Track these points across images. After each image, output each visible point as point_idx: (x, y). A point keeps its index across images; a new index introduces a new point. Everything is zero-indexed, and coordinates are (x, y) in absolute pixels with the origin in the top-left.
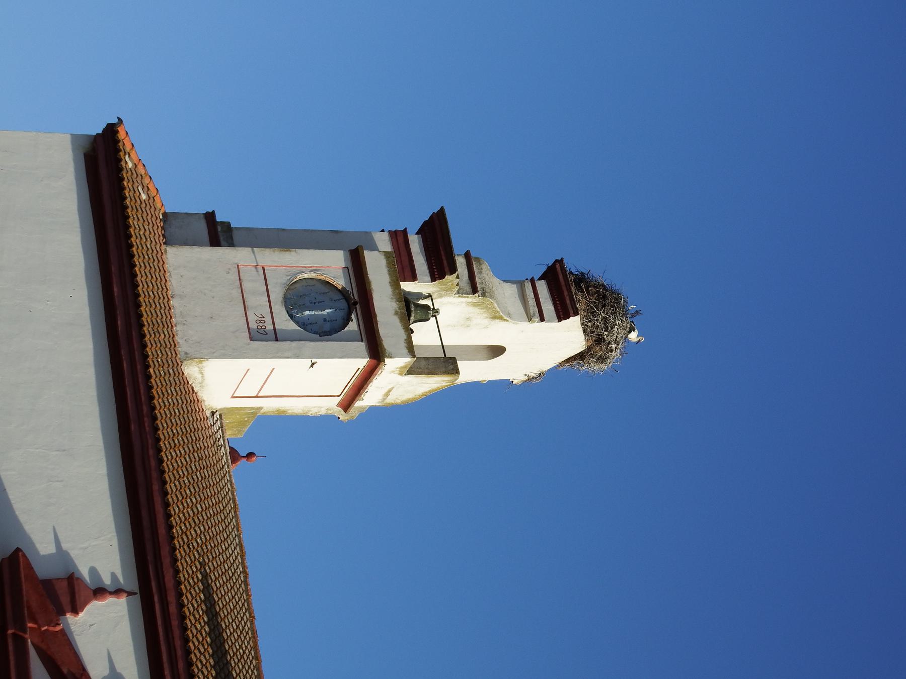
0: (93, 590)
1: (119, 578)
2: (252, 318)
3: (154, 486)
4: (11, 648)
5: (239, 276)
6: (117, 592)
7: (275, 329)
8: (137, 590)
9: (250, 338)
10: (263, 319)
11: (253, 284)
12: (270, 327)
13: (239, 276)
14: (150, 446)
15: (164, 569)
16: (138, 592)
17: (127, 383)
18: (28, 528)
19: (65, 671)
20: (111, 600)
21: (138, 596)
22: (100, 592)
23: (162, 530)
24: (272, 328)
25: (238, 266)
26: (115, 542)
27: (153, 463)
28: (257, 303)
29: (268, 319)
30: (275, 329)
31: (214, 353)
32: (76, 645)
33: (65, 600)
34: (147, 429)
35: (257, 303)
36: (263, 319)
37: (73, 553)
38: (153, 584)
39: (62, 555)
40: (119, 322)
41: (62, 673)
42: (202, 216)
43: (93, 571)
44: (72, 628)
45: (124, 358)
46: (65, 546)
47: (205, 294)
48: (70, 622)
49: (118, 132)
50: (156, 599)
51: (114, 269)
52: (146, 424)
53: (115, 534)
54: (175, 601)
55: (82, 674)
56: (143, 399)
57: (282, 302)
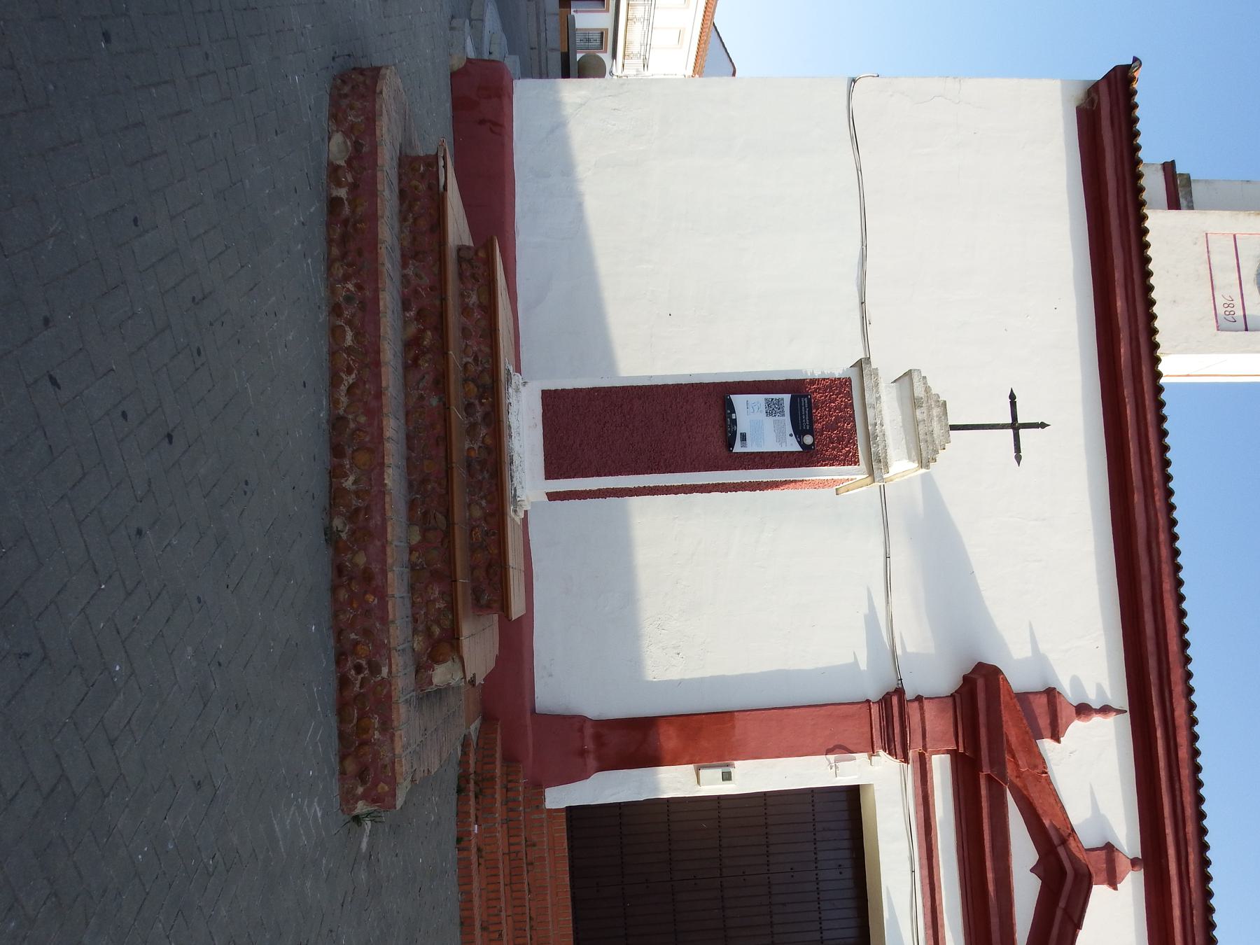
0: (1075, 707)
1: (1106, 691)
2: (1220, 301)
3: (1164, 585)
4: (984, 792)
5: (1208, 247)
6: (1105, 710)
7: (1245, 316)
8: (1127, 708)
9: (1218, 327)
10: (1232, 302)
11: (1222, 258)
12: (1239, 313)
13: (1208, 247)
14: (1161, 530)
15: (1174, 700)
16: (1128, 711)
17: (1130, 435)
18: (999, 623)
19: (1047, 822)
20: (1097, 719)
21: (1127, 715)
22: (1083, 710)
23: (1173, 646)
24: (1241, 313)
25: (1207, 234)
26: (1102, 643)
27: (1165, 552)
28: (1226, 279)
29: (1238, 302)
30: (1245, 316)
31: (1176, 346)
32: (1054, 778)
33: (1044, 722)
34: (1158, 504)
35: (1226, 279)
36: (1232, 302)
37: (1052, 657)
38: (1157, 714)
39: (1039, 658)
40: (1122, 351)
41: (1042, 825)
42: (1160, 167)
43: (1076, 682)
44: (1049, 755)
45: (1127, 400)
46: (1043, 647)
47: (1168, 272)
48: (1047, 748)
49: (1133, 79)
50: (1159, 733)
51: (1118, 275)
52: (1157, 498)
53: (1102, 632)
54: (1186, 743)
55: (1070, 834)
56: (1154, 462)
57: (1254, 281)
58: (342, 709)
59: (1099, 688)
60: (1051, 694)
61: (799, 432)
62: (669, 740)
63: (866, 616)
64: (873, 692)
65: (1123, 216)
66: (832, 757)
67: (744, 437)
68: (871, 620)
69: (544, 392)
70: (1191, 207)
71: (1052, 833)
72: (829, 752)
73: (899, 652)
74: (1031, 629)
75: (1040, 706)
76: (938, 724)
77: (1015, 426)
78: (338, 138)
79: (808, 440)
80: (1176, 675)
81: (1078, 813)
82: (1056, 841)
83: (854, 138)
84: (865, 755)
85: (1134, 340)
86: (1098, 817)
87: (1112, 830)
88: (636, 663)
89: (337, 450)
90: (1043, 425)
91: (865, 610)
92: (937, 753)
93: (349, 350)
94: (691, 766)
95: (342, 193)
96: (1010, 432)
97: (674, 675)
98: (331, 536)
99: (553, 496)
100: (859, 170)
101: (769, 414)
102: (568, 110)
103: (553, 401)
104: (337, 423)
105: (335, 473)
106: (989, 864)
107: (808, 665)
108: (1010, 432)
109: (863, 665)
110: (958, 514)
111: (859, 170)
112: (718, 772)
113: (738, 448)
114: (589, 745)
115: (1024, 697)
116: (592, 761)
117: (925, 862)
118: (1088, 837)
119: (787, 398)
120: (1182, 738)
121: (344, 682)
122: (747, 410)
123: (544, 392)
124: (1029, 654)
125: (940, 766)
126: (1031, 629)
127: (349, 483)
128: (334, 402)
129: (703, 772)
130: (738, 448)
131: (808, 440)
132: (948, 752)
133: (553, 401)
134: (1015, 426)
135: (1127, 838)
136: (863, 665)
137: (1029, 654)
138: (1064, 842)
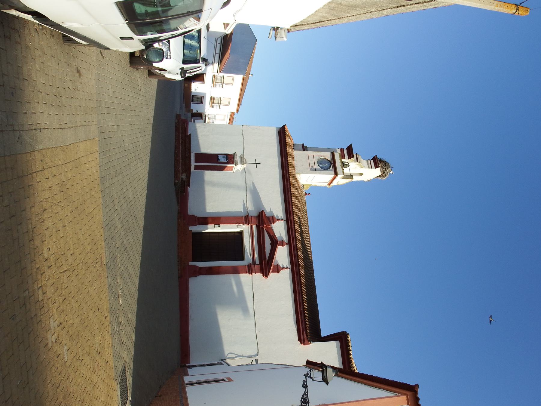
11: (311, 159)
20: (280, 221)
22: (278, 220)
23: (291, 208)
33: (272, 221)
39: (271, 212)
58: (175, 171)
59: (281, 216)
60: (273, 217)
61: (226, 160)
62: (210, 220)
63: (243, 204)
64: (244, 215)
65: (284, 146)
66: (237, 225)
67: (220, 160)
68: (244, 205)
69: (195, 154)
70: (307, 151)
71: (272, 236)
72: (236, 224)
73: (248, 210)
74: (270, 208)
75: (271, 219)
76: (254, 220)
77: (256, 163)
78: (177, 120)
79: (228, 161)
80: (291, 212)
81: (277, 235)
82: (273, 237)
83: (243, 134)
84: (242, 224)
85: (286, 164)
86: (281, 236)
87: (283, 238)
88: (205, 209)
89: (175, 148)
90: (256, 160)
91: (243, 203)
92: (254, 225)
93: (177, 140)
94: (213, 225)
95: (177, 125)
96: (255, 164)
97: (211, 211)
98: (175, 157)
99: (216, 38)
100: (243, 138)
101: (223, 157)
102: (197, 127)
103: (196, 154)
104: (175, 146)
105: (175, 150)
106: (262, 241)
107: (233, 211)
108: (255, 164)
109: (242, 212)
110: (258, 190)
111: (243, 138)
112: (218, 226)
113: (219, 161)
114: (197, 220)
115: (268, 217)
116: (197, 223)
117: (252, 242)
118: (279, 239)
119: (225, 156)
120: (292, 221)
121: (175, 169)
122: (220, 157)
123: (195, 154)
124: (270, 211)
125: (254, 227)
126: (270, 208)
127: (176, 151)
128: (175, 144)
129: (215, 226)
130: (219, 161)
131: (228, 161)
132: (256, 225)
133: (196, 154)
134: (256, 163)
135: (285, 238)
136: (242, 212)
137: (270, 211)
138: (274, 237)
